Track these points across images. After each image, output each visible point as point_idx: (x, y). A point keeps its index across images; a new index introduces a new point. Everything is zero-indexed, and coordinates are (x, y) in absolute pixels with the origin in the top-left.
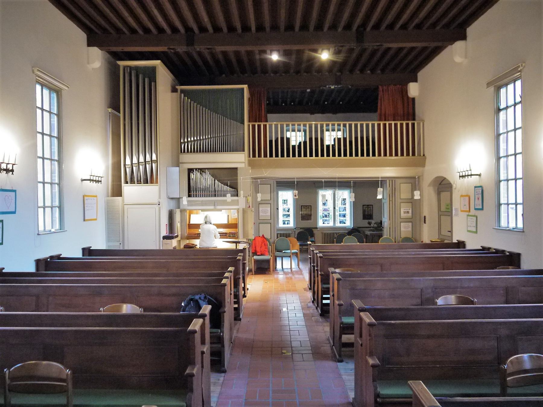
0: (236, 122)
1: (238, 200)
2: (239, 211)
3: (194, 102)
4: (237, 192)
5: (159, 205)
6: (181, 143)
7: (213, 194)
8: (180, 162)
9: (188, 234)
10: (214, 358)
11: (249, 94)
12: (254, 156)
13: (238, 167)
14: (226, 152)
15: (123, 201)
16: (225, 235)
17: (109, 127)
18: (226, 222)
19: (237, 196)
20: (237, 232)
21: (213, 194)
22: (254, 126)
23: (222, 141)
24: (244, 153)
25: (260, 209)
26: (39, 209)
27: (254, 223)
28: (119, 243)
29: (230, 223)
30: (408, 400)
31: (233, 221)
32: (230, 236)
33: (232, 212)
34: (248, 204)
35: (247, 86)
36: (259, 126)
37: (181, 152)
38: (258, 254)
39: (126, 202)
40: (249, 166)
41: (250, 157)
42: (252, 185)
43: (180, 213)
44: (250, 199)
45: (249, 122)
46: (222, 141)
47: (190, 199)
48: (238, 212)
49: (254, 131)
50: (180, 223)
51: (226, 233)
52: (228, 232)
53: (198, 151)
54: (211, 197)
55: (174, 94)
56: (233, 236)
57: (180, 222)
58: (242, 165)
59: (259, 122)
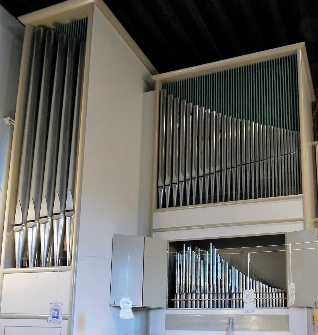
0: (279, 128)
1: (287, 317)
3: (200, 107)
5: (57, 318)
6: (158, 187)
7: (225, 301)
11: (314, 96)
13: (286, 232)
14: (255, 197)
17: (5, 164)
19: (286, 306)
21: (225, 301)
23: (255, 178)
24: (299, 197)
26: (301, 216)
35: (303, 44)
37: (158, 207)
40: (315, 227)
45: (315, 140)
46: (255, 178)
47: (172, 312)
53: (205, 201)
54: (221, 307)
58: (299, 227)
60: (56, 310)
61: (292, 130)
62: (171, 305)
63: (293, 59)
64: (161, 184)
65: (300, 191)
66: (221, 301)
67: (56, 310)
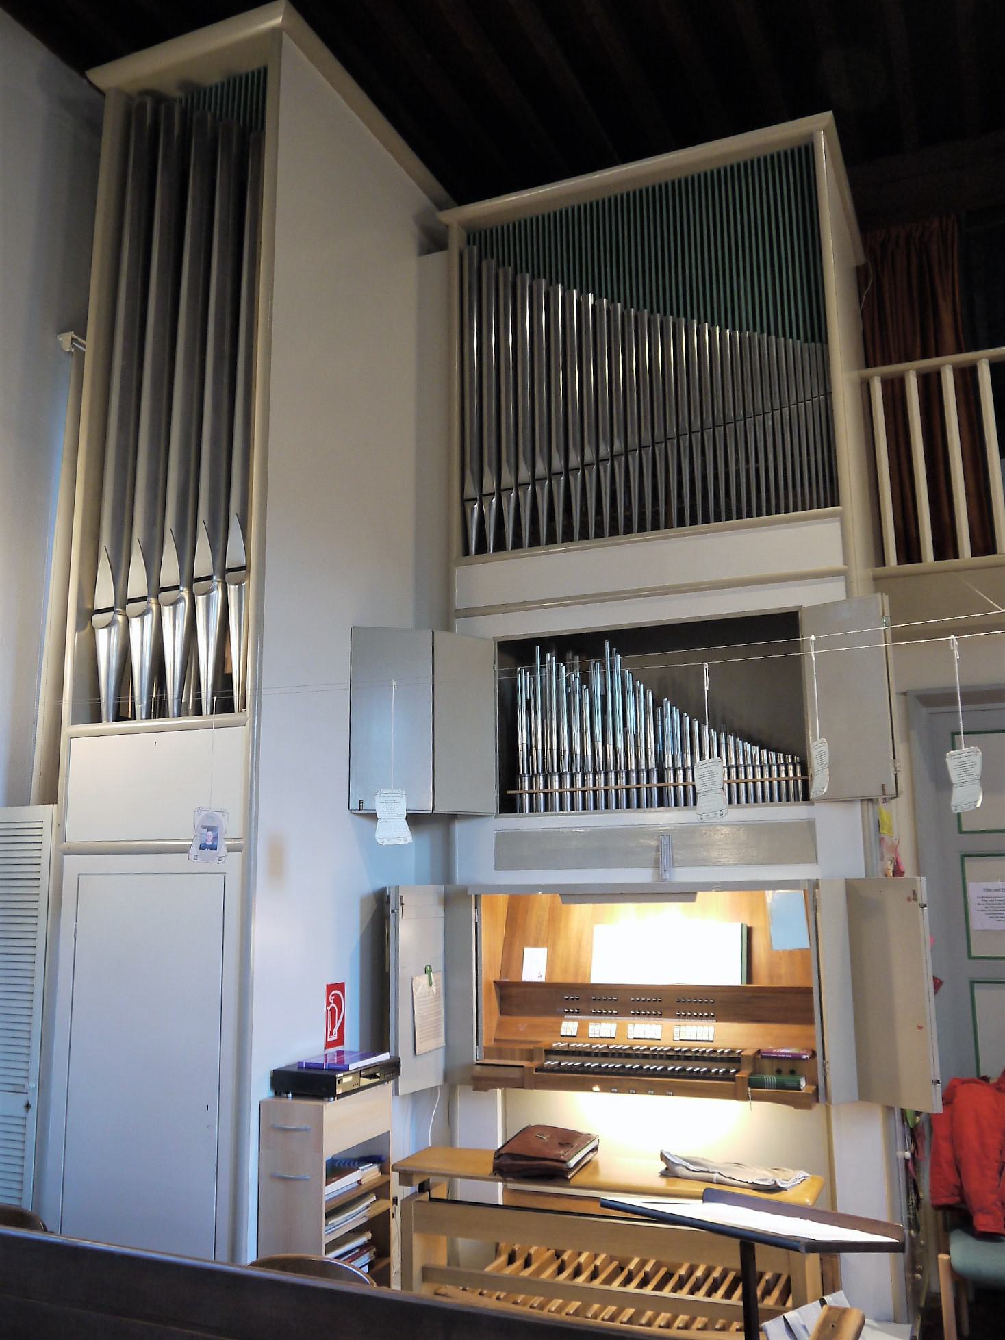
0: (773, 337)
1: (811, 825)
2: (823, 895)
4: (805, 771)
5: (213, 848)
7: (649, 790)
8: (863, 877)
9: (488, 1052)
10: (963, 746)
11: (860, 250)
12: (909, 551)
15: (62, 826)
16: (727, 1076)
18: (731, 975)
20: (814, 1054)
21: (649, 790)
22: (895, 393)
25: (975, 889)
26: (838, 564)
27: (937, 984)
28: (22, 1099)
29: (762, 980)
30: (800, 785)
31: (783, 970)
32: (760, 1085)
33: (769, 900)
34: (888, 856)
35: (825, 118)
36: (930, 386)
37: (466, 552)
38: (983, 1222)
39: (75, 835)
40: (876, 592)
41: (881, 560)
42: (908, 739)
43: (442, 913)
44: (898, 816)
45: (868, 366)
47: (511, 823)
48: (812, 907)
49: (907, 482)
50: (438, 977)
51: (733, 1059)
52: (749, 1052)
54: (639, 806)
55: (438, 257)
56: (780, 1086)
57: (439, 966)
58: (833, 591)
59: (925, 356)
60: (209, 829)
61: (806, 340)
62: (508, 805)
63: (804, 154)
64: (471, 491)
65: (832, 498)
66: (638, 790)
67: (209, 829)
